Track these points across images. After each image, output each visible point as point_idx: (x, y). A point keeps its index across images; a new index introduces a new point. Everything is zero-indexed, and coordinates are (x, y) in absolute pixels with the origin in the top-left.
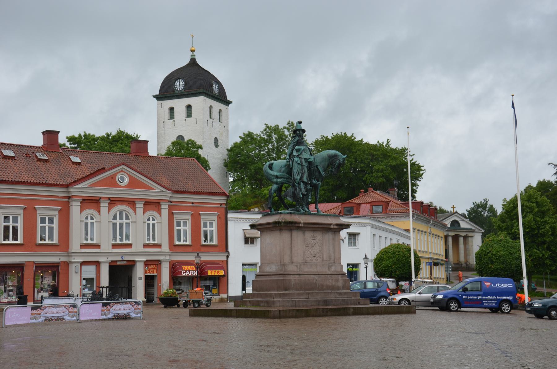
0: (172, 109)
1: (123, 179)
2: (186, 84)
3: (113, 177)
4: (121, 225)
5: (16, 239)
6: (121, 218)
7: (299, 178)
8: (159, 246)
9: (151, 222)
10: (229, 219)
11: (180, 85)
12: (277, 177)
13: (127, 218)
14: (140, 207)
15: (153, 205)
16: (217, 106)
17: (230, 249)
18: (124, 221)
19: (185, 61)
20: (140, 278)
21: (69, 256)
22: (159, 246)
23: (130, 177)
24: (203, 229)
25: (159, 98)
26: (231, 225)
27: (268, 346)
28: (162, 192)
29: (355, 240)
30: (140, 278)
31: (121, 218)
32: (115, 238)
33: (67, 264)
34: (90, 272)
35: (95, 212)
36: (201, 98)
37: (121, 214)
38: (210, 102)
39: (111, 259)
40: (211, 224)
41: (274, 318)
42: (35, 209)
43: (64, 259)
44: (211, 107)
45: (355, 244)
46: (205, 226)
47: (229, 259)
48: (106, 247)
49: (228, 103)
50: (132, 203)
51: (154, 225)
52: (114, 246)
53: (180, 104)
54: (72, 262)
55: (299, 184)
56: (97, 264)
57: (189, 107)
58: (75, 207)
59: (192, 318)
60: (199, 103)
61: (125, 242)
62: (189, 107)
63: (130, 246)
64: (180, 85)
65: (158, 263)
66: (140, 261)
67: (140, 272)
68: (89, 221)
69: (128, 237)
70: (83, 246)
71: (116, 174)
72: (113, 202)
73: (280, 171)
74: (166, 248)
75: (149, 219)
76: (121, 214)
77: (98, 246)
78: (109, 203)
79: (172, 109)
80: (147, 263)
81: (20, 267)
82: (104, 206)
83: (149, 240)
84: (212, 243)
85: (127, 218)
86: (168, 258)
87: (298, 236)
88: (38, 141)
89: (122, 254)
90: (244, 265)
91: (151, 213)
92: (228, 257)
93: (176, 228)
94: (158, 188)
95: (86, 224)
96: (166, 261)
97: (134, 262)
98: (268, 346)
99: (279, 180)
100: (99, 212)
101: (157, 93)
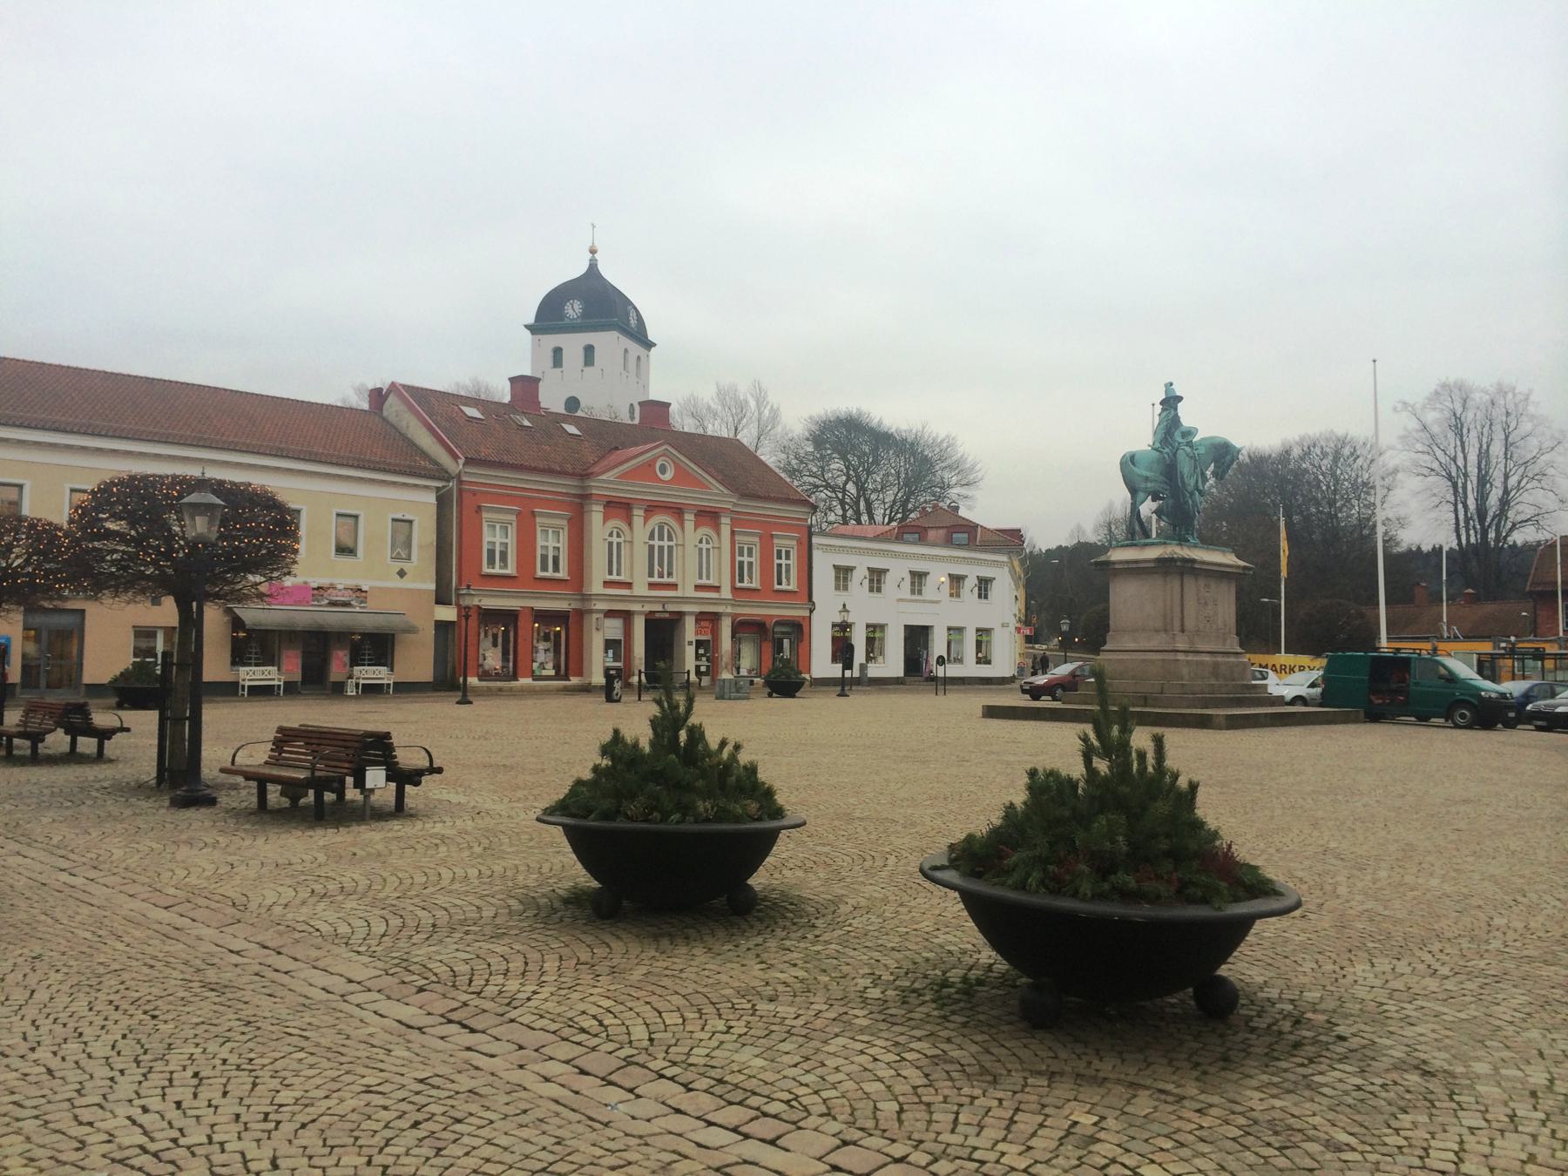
0: (558, 352)
1: (663, 470)
3: (650, 464)
4: (661, 548)
5: (506, 566)
7: (1192, 482)
8: (717, 589)
9: (615, 540)
11: (573, 309)
12: (1147, 479)
14: (689, 517)
15: (709, 516)
16: (635, 349)
20: (690, 643)
22: (717, 589)
23: (678, 468)
26: (816, 554)
27: (1466, 801)
28: (723, 495)
30: (690, 643)
33: (581, 614)
34: (614, 629)
35: (624, 526)
36: (613, 335)
37: (661, 529)
38: (627, 342)
39: (648, 608)
42: (533, 514)
43: (575, 605)
45: (846, 588)
48: (641, 589)
49: (649, 345)
50: (678, 511)
51: (619, 544)
53: (573, 344)
54: (591, 612)
56: (627, 616)
58: (596, 515)
59: (990, 721)
60: (608, 343)
61: (666, 580)
63: (674, 586)
64: (573, 309)
65: (714, 618)
67: (690, 631)
68: (615, 540)
70: (607, 584)
71: (655, 460)
73: (1151, 470)
74: (726, 593)
75: (611, 535)
76: (661, 529)
77: (629, 585)
79: (558, 352)
80: (701, 617)
82: (638, 513)
84: (557, 575)
85: (670, 539)
86: (729, 610)
87: (1191, 585)
89: (664, 601)
90: (949, 629)
91: (705, 530)
92: (811, 611)
93: (738, 558)
94: (717, 488)
97: (681, 614)
98: (1466, 801)
101: (531, 320)
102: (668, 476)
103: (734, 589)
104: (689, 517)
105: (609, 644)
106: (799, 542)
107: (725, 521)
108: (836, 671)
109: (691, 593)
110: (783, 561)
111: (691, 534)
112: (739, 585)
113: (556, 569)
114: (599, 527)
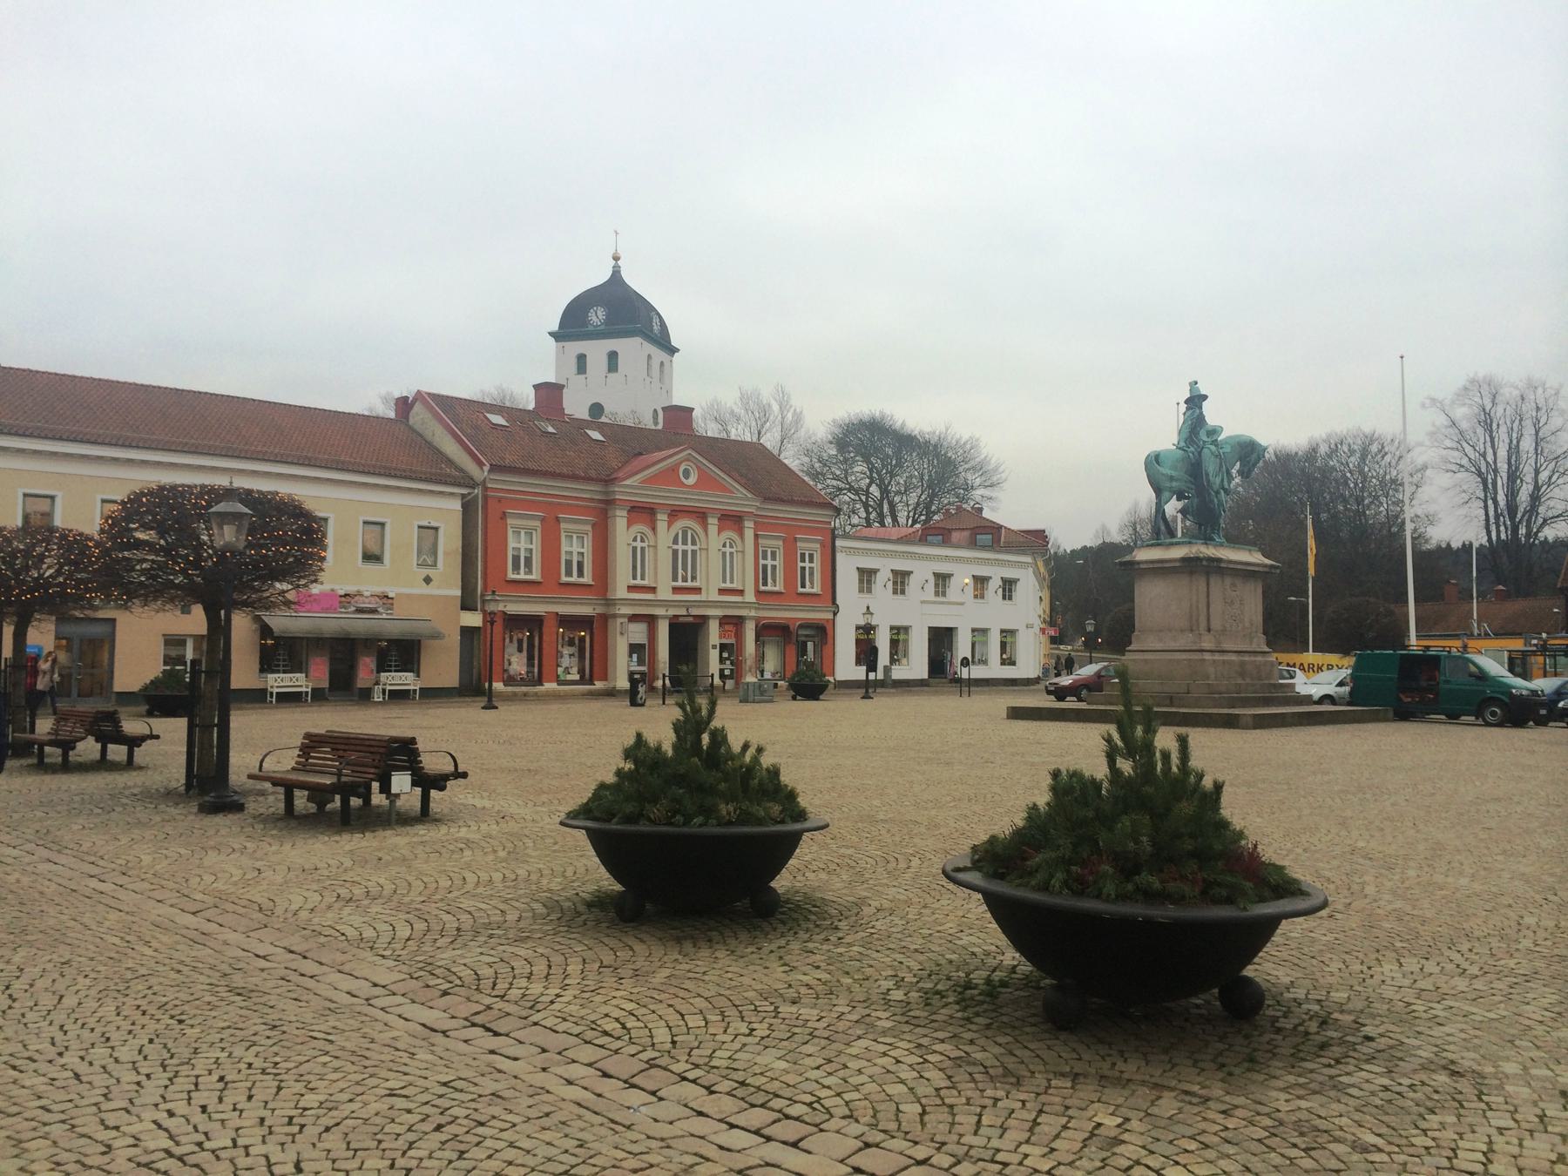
0: (582, 359)
1: (687, 474)
2: (608, 316)
4: (685, 553)
6: (685, 543)
7: (1218, 480)
8: (741, 592)
9: (728, 550)
11: (597, 316)
12: (1172, 478)
14: (713, 522)
15: (732, 520)
16: (659, 355)
17: (838, 602)
20: (714, 647)
21: (607, 605)
22: (741, 592)
25: (557, 336)
28: (747, 499)
30: (714, 647)
31: (685, 543)
32: (675, 579)
33: (605, 619)
34: (638, 633)
39: (672, 612)
43: (600, 610)
44: (649, 357)
46: (803, 560)
49: (672, 351)
50: (701, 516)
52: (676, 590)
53: (596, 350)
54: (615, 616)
55: (1217, 493)
56: (651, 620)
57: (613, 356)
58: (620, 520)
60: (632, 349)
61: (689, 584)
62: (613, 356)
63: (697, 590)
64: (597, 316)
67: (714, 635)
69: (694, 578)
70: (631, 588)
72: (675, 513)
74: (750, 597)
77: (653, 590)
79: (582, 359)
80: (724, 621)
81: (534, 622)
82: (662, 518)
83: (634, 578)
85: (694, 543)
86: (753, 613)
89: (688, 605)
90: (973, 630)
92: (835, 614)
93: (762, 562)
95: (635, 549)
97: (705, 618)
100: (654, 529)
101: (555, 328)
102: (692, 480)
103: (758, 593)
104: (713, 522)
105: (634, 648)
106: (823, 545)
107: (749, 524)
110: (807, 565)
111: (715, 538)
112: (762, 588)
113: (581, 574)
114: (623, 533)
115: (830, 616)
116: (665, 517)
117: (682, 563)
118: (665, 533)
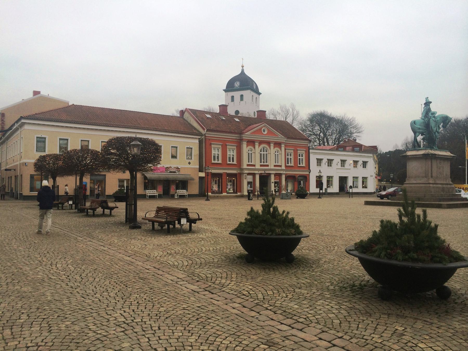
0: (233, 97)
5: (218, 161)
6: (264, 151)
7: (435, 129)
8: (281, 166)
10: (310, 153)
11: (237, 84)
12: (419, 129)
13: (266, 152)
14: (272, 145)
15: (278, 145)
16: (255, 95)
18: (265, 153)
19: (239, 72)
20: (273, 182)
22: (281, 166)
23: (268, 130)
24: (299, 158)
25: (225, 91)
28: (282, 138)
29: (320, 163)
30: (273, 182)
31: (264, 151)
37: (264, 148)
39: (260, 172)
40: (291, 155)
41: (445, 208)
42: (226, 145)
46: (300, 156)
47: (311, 174)
49: (259, 94)
50: (268, 143)
53: (237, 95)
54: (243, 173)
56: (254, 175)
57: (242, 96)
58: (244, 145)
60: (247, 94)
61: (265, 164)
62: (242, 96)
63: (268, 166)
64: (237, 84)
65: (280, 175)
66: (273, 174)
67: (273, 179)
68: (277, 153)
69: (266, 162)
70: (248, 165)
71: (262, 128)
72: (261, 143)
74: (283, 167)
76: (264, 148)
77: (254, 166)
78: (259, 143)
79: (233, 97)
80: (276, 175)
81: (220, 175)
82: (257, 144)
85: (266, 152)
86: (284, 172)
88: (217, 110)
90: (353, 177)
92: (310, 173)
93: (287, 157)
96: (257, 174)
97: (270, 174)
99: (420, 130)
101: (225, 88)
102: (266, 133)
103: (286, 166)
104: (272, 145)
105: (249, 183)
106: (306, 152)
108: (317, 190)
109: (273, 167)
110: (301, 158)
111: (273, 150)
112: (287, 165)
113: (233, 161)
114: (245, 149)
115: (308, 173)
116: (258, 144)
117: (263, 158)
118: (258, 148)
